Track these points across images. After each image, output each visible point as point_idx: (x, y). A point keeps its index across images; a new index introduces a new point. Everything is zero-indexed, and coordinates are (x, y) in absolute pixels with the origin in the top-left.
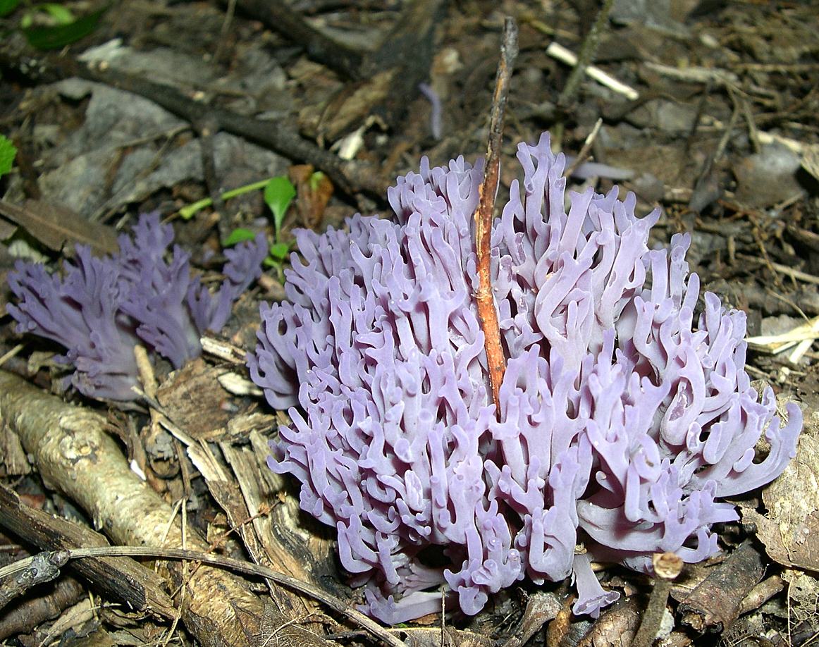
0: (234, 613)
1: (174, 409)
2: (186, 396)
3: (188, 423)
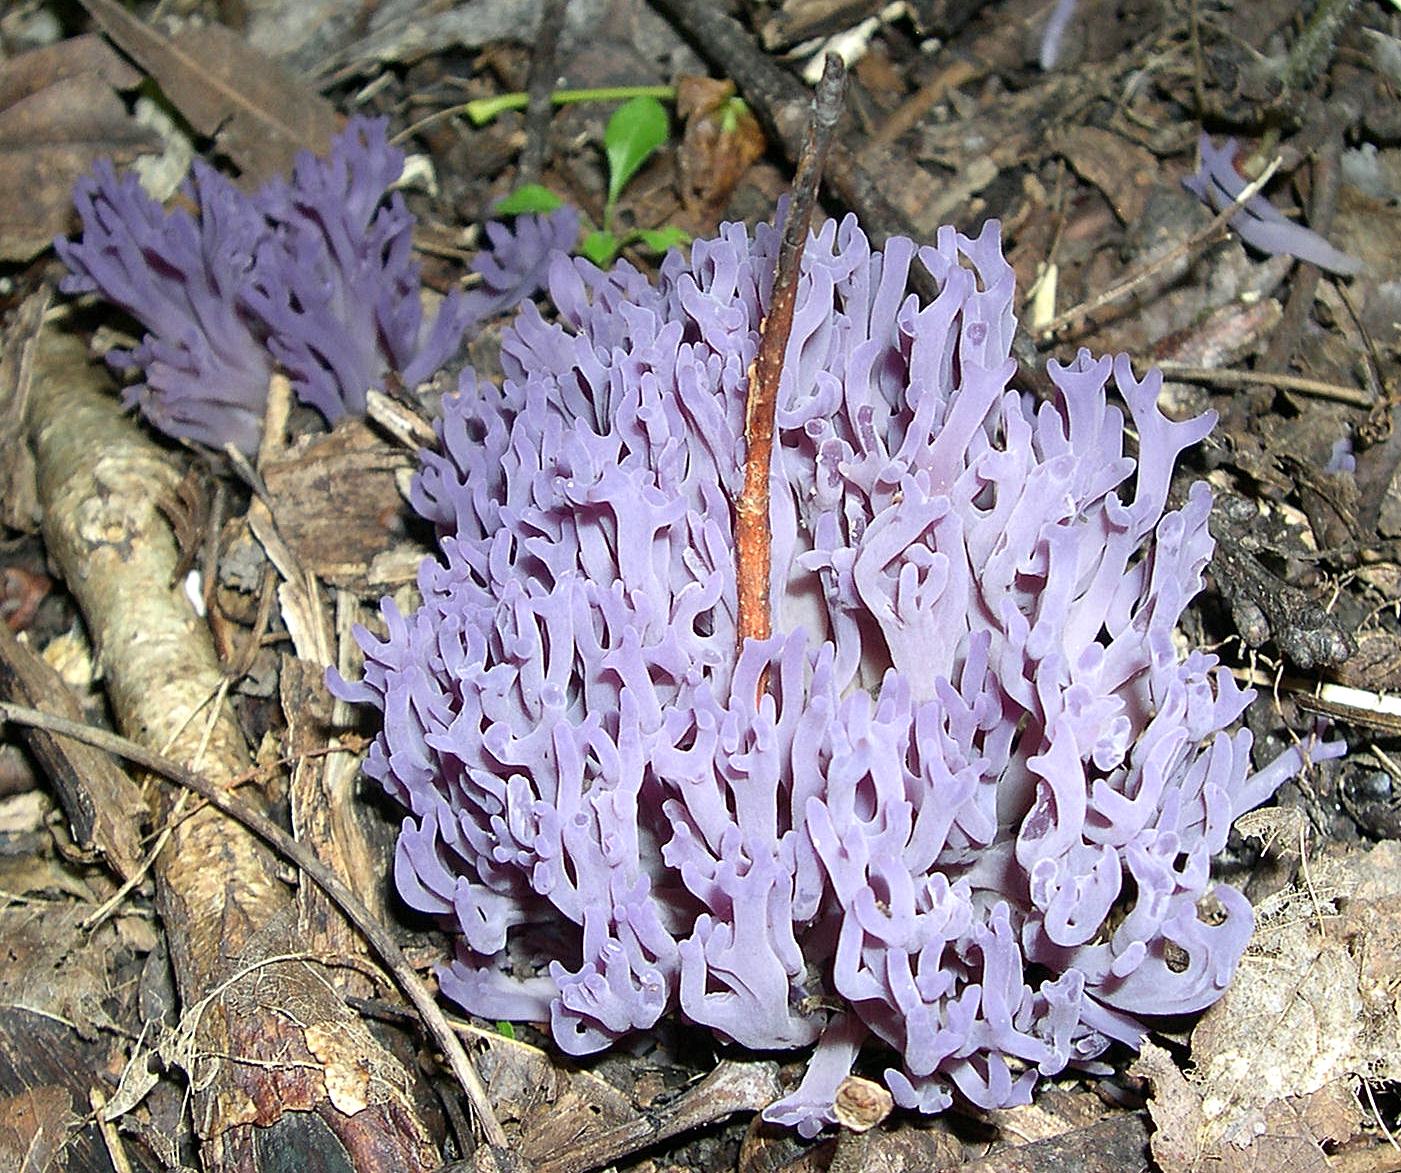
0: (222, 906)
1: (290, 503)
2: (321, 484)
3: (303, 536)
